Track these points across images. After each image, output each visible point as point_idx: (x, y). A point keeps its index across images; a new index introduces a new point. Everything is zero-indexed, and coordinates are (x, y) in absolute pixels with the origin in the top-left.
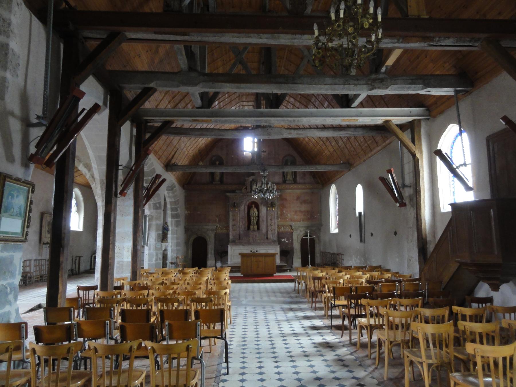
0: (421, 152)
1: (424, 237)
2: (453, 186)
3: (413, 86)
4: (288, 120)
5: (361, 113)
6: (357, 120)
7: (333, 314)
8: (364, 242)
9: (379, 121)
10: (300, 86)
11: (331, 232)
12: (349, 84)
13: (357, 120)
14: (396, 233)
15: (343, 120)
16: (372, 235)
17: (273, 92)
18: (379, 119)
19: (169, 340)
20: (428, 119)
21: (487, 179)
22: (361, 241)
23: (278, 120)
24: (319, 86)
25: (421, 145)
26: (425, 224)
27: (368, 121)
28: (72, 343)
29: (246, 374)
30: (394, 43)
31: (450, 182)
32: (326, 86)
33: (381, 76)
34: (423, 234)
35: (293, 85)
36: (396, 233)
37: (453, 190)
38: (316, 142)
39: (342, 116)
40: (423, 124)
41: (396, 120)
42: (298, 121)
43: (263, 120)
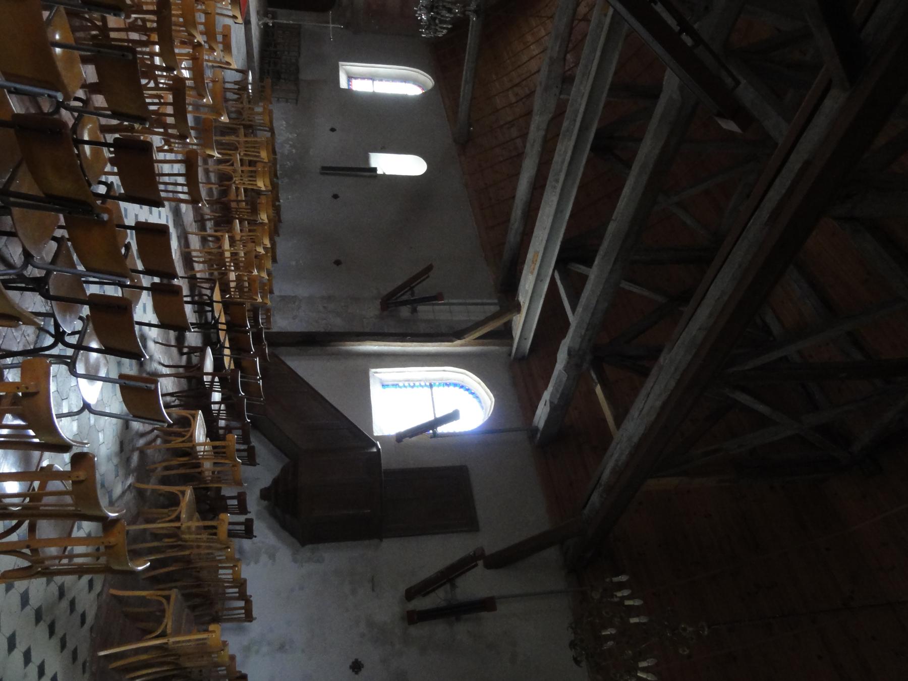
0: (462, 345)
1: (332, 344)
2: (406, 384)
3: (558, 396)
4: (560, 171)
5: (541, 281)
6: (532, 273)
7: (188, 294)
8: (322, 174)
9: (524, 298)
10: (609, 267)
11: (341, 63)
12: (587, 330)
13: (532, 273)
14: (338, 263)
15: (537, 253)
16: (336, 196)
17: (612, 222)
18: (525, 300)
19: (81, 66)
20: (510, 355)
21: (412, 465)
22: (324, 168)
23: (566, 152)
24: (599, 293)
25: (472, 345)
26: (353, 345)
27: (527, 286)
28: (67, 244)
29: (90, 592)
30: (617, 461)
31: (412, 381)
32: (594, 302)
33: (585, 366)
34: (336, 343)
35: (613, 259)
36: (338, 263)
37: (401, 384)
38: (519, 66)
39: (544, 254)
40: (505, 349)
41: (518, 321)
42: (555, 187)
43: (574, 126)
